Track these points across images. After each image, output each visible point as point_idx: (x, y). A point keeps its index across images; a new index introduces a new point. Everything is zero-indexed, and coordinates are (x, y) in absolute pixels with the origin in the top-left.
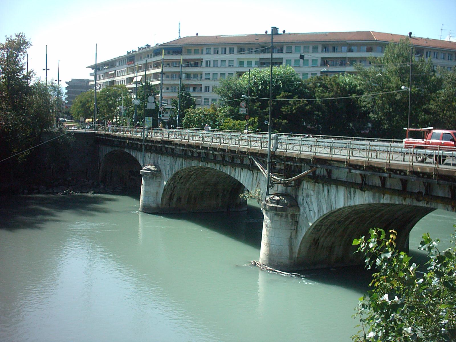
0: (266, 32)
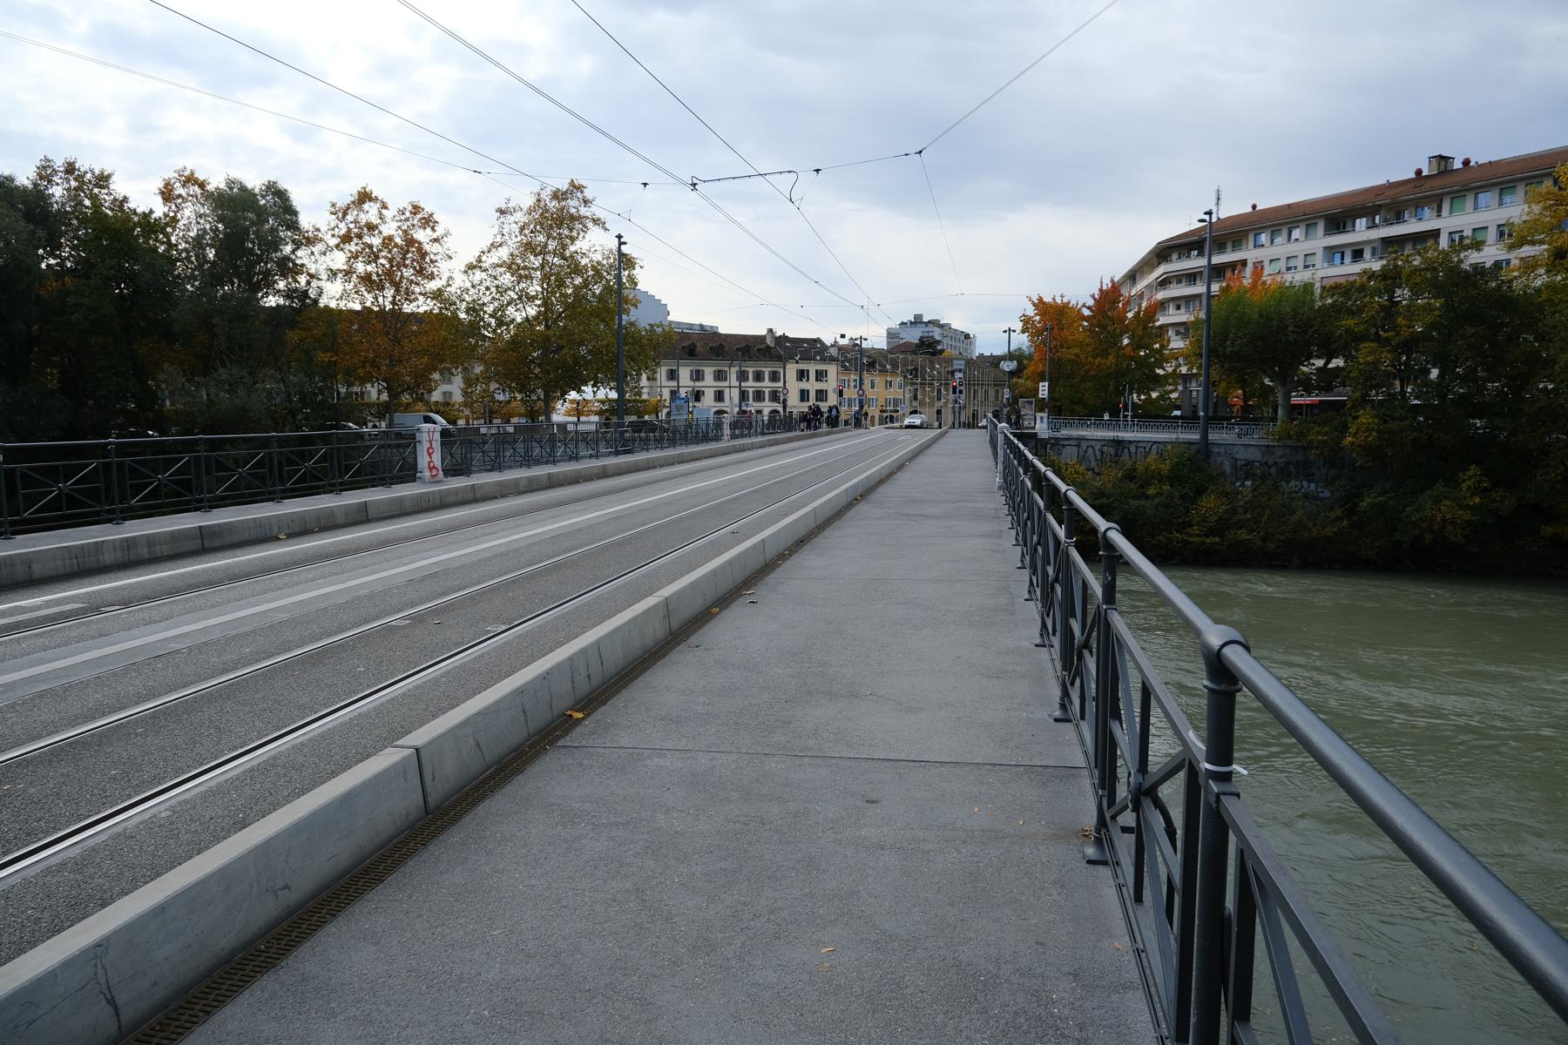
0: (1419, 172)
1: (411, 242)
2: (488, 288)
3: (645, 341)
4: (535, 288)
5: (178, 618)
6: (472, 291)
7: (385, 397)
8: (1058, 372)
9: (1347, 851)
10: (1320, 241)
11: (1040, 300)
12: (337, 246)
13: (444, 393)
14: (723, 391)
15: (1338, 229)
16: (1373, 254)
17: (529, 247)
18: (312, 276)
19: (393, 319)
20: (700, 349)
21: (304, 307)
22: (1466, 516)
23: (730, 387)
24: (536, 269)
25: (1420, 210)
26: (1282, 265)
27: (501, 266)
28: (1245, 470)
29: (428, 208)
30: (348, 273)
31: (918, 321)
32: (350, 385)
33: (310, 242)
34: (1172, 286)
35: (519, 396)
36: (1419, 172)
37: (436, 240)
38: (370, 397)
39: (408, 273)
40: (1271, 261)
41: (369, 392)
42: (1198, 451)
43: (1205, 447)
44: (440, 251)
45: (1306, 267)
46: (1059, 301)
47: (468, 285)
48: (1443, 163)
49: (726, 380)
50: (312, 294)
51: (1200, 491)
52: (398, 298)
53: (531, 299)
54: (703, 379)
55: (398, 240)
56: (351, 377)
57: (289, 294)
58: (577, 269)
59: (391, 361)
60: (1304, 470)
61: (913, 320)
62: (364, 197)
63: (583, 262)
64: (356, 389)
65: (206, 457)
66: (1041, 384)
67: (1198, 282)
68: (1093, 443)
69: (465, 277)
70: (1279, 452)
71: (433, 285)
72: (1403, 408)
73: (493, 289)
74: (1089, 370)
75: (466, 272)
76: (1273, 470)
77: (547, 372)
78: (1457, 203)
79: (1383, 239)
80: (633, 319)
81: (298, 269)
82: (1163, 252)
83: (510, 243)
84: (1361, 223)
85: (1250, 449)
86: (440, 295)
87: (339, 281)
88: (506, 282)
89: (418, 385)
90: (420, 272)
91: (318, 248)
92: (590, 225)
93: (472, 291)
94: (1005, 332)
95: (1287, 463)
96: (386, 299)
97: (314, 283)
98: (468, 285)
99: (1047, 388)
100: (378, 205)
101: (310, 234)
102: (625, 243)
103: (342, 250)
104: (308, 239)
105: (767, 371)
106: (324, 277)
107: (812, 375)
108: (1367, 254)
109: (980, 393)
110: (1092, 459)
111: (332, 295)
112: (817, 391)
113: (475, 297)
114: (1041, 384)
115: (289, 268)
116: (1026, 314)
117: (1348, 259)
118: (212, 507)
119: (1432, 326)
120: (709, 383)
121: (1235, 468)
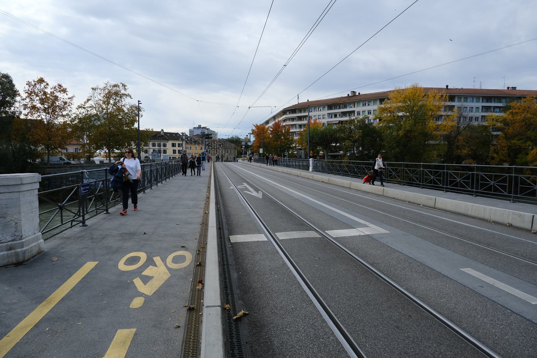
0: (348, 95)
10: (326, 112)
11: (257, 125)
14: (147, 150)
15: (331, 108)
16: (339, 116)
21: (13, 118)
23: (150, 149)
25: (350, 105)
26: (317, 117)
29: (64, 86)
31: (199, 127)
34: (287, 121)
36: (348, 95)
40: (314, 116)
45: (323, 118)
48: (354, 93)
49: (148, 146)
61: (198, 127)
62: (41, 81)
65: (477, 174)
66: (260, 149)
67: (295, 120)
72: (354, 157)
74: (273, 145)
78: (358, 104)
82: (284, 112)
94: (249, 134)
99: (262, 150)
100: (45, 84)
102: (141, 103)
107: (177, 145)
108: (338, 116)
109: (229, 151)
112: (178, 150)
114: (260, 149)
116: (253, 129)
117: (333, 117)
118: (404, 185)
119: (360, 136)
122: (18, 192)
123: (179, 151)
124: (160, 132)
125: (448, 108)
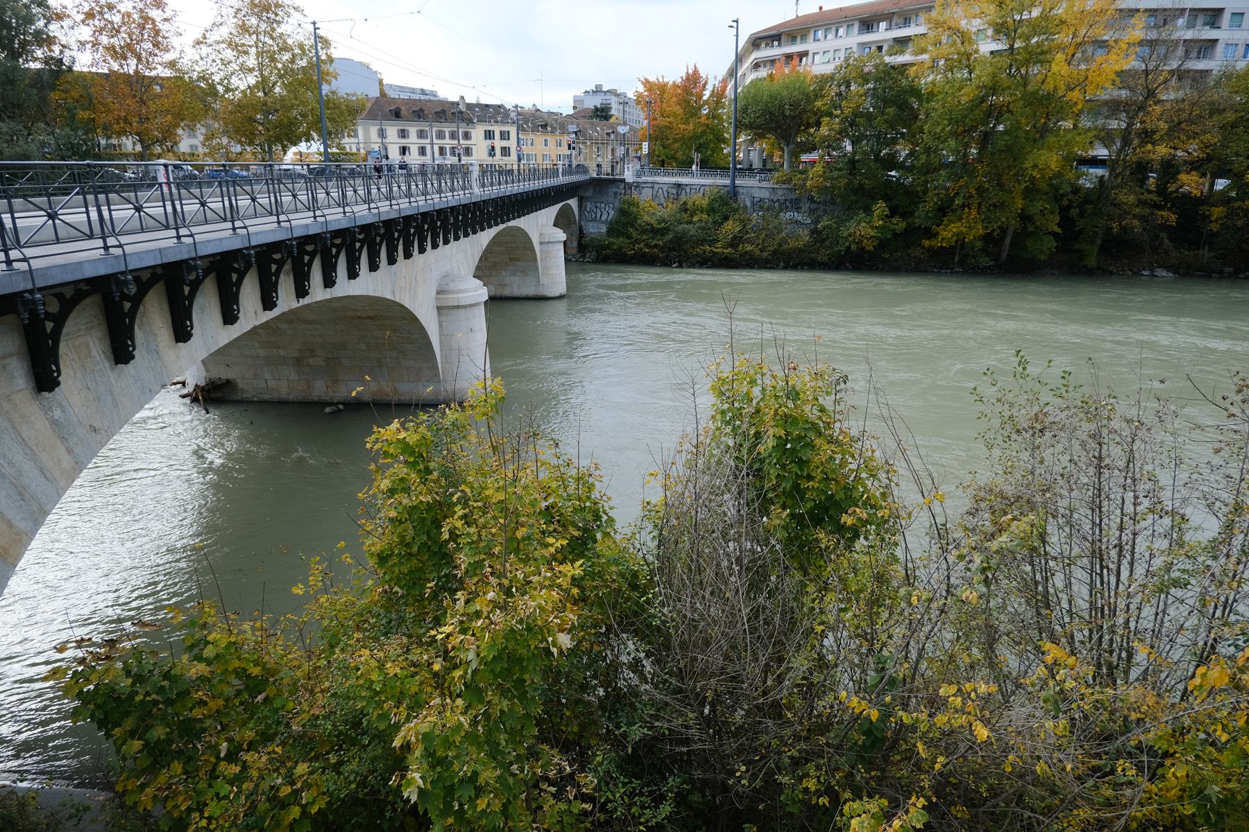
1: (146, 19)
2: (214, 61)
3: (343, 107)
4: (251, 62)
5: (64, 450)
6: (201, 63)
7: (139, 148)
8: (658, 135)
9: (1122, 568)
12: (83, 21)
13: (191, 146)
17: (244, 29)
18: (64, 46)
19: (139, 84)
20: (404, 112)
21: (57, 72)
22: (872, 233)
24: (250, 46)
27: (223, 42)
28: (759, 204)
30: (95, 44)
31: (598, 90)
32: (109, 137)
33: (59, 17)
35: (249, 149)
37: (166, 20)
38: (126, 148)
39: (148, 45)
41: (126, 145)
42: (728, 192)
43: (734, 191)
44: (171, 28)
46: (661, 80)
47: (197, 57)
50: (66, 61)
51: (726, 218)
52: (140, 66)
53: (251, 70)
54: (471, 138)
55: (136, 16)
56: (108, 131)
57: (47, 61)
58: (285, 48)
59: (141, 119)
60: (795, 205)
63: (290, 41)
64: (114, 141)
68: (662, 186)
69: (194, 51)
70: (780, 193)
71: (168, 57)
73: (219, 62)
75: (194, 47)
76: (777, 205)
77: (268, 130)
79: (894, 39)
80: (334, 89)
81: (50, 41)
83: (229, 23)
84: (883, 25)
85: (763, 190)
86: (174, 66)
87: (88, 52)
88: (228, 55)
89: (165, 139)
90: (156, 45)
91: (67, 23)
92: (292, 11)
93: (201, 63)
95: (785, 200)
96: (131, 66)
97: (67, 53)
98: (197, 57)
101: (59, 11)
103: (88, 25)
104: (57, 14)
105: (447, 131)
106: (75, 47)
107: (497, 135)
110: (662, 197)
111: (84, 62)
113: (204, 68)
115: (44, 39)
120: (413, 140)
121: (753, 203)
122: (125, 260)
123: (453, 149)
124: (458, 104)
125: (1200, 20)
